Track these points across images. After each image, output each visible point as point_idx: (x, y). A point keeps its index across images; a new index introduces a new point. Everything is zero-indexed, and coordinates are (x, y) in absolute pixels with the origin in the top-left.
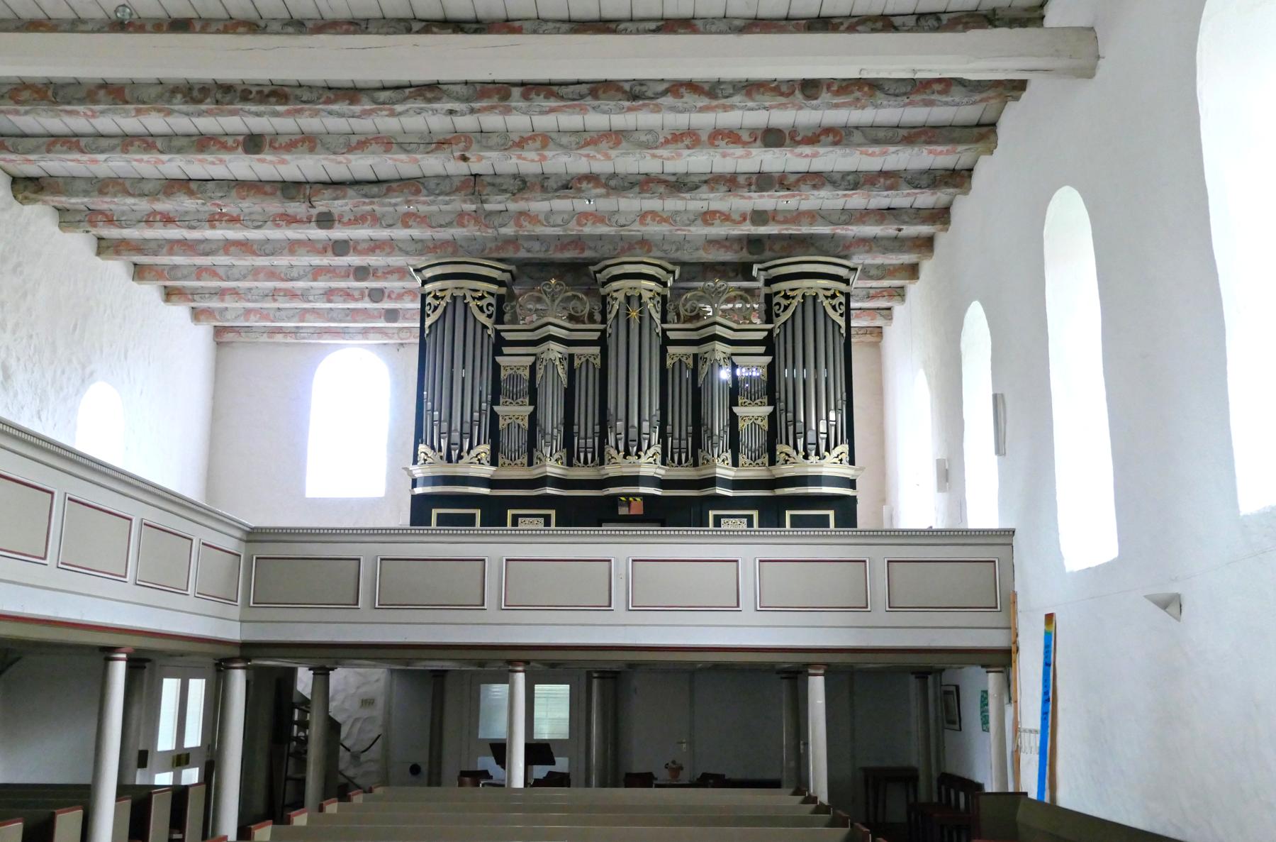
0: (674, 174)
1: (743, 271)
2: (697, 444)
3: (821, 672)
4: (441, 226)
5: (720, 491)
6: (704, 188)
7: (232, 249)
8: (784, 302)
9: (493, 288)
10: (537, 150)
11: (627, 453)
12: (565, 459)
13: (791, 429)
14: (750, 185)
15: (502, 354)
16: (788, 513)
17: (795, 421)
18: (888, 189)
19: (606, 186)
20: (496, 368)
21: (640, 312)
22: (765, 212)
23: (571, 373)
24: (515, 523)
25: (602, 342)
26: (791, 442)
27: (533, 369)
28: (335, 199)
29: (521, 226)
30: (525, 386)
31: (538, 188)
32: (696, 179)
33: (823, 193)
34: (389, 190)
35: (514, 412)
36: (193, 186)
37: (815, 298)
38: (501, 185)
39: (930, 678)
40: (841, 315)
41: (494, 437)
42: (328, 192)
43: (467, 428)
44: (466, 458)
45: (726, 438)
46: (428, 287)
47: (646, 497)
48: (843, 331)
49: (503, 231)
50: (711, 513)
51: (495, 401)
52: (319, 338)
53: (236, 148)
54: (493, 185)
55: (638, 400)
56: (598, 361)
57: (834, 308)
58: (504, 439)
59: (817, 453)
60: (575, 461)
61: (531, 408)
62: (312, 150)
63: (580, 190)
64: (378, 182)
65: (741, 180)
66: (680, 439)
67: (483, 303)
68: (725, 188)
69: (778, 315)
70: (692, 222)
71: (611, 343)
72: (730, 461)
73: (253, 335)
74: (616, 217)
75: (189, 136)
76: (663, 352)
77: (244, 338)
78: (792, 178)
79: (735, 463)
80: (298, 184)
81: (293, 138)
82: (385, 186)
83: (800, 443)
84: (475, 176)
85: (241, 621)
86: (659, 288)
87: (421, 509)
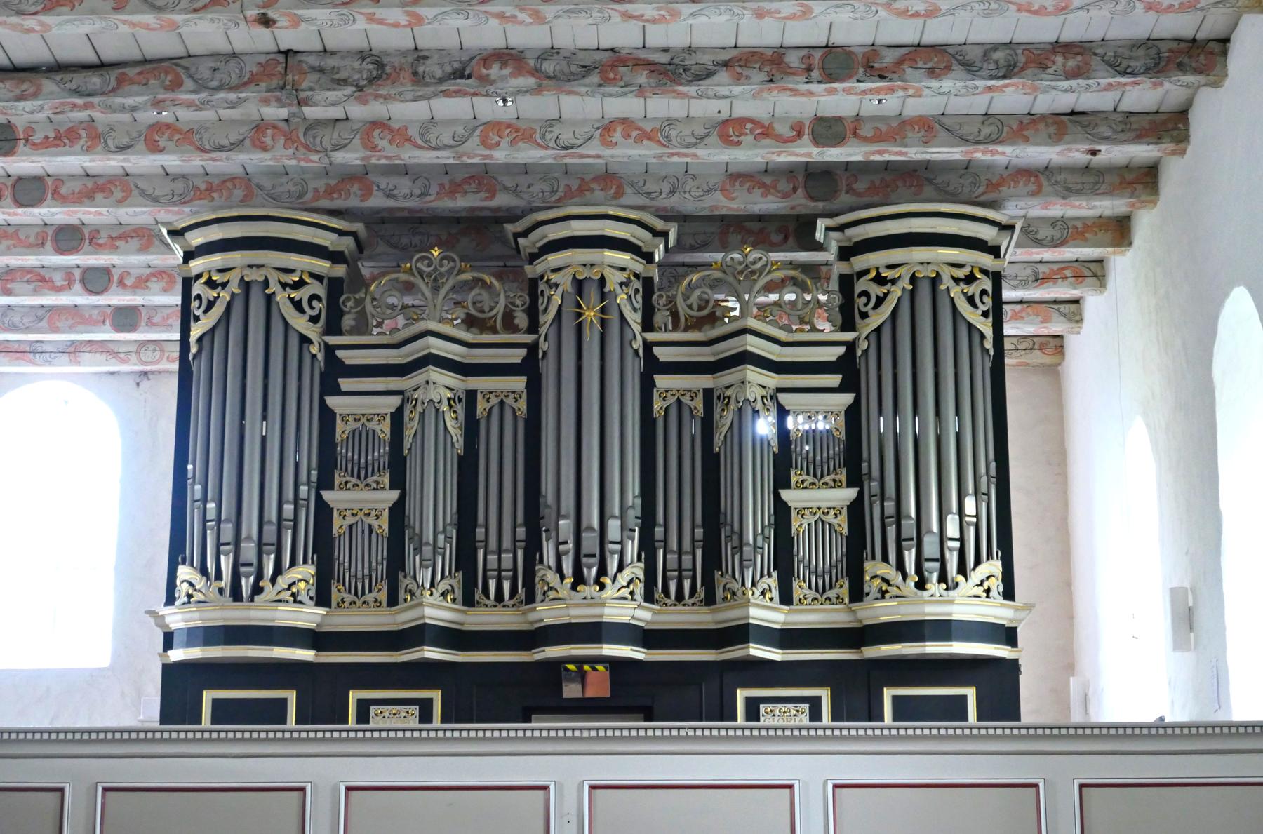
1: (799, 231)
2: (713, 561)
4: (220, 149)
5: (757, 651)
6: (723, 76)
8: (876, 290)
9: (322, 266)
11: (579, 579)
12: (459, 594)
13: (891, 531)
14: (809, 69)
15: (338, 392)
16: (208, 696)
17: (899, 515)
19: (536, 72)
20: (327, 417)
22: (839, 120)
23: (471, 427)
24: (363, 717)
25: (530, 367)
26: (892, 557)
27: (397, 419)
28: (20, 98)
30: (381, 453)
31: (406, 76)
32: (706, 59)
33: (947, 84)
34: (121, 81)
37: (935, 281)
40: (985, 314)
43: (270, 533)
44: (269, 592)
45: (768, 549)
46: (197, 265)
47: (616, 665)
48: (989, 344)
49: (340, 157)
50: (741, 694)
51: (325, 482)
54: (321, 71)
55: (601, 480)
56: (522, 405)
57: (971, 300)
58: (341, 554)
59: (943, 578)
60: (478, 595)
63: (485, 80)
64: (101, 66)
65: (793, 59)
66: (680, 552)
67: (302, 294)
69: (864, 316)
70: (701, 140)
71: (547, 369)
72: (775, 593)
74: (556, 131)
78: (889, 57)
79: (786, 598)
82: (115, 73)
83: (910, 558)
84: (287, 53)
86: (638, 265)
87: (181, 690)
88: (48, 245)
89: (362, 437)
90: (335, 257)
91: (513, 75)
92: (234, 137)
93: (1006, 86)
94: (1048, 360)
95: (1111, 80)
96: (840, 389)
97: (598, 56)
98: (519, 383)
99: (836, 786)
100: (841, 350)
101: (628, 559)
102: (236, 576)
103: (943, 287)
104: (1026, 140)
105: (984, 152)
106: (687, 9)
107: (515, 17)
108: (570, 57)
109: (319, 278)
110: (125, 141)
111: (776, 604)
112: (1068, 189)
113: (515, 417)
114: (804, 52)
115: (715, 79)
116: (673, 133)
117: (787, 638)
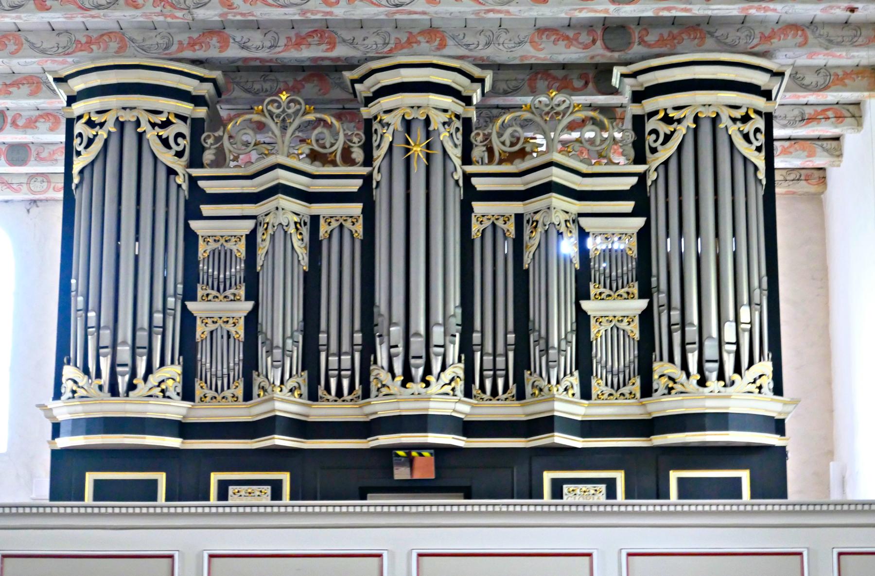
2: (523, 362)
5: (561, 439)
8: (664, 129)
9: (186, 108)
11: (408, 377)
13: (677, 337)
15: (200, 217)
21: (428, 146)
23: (315, 247)
27: (251, 239)
30: (238, 269)
37: (715, 121)
40: (759, 149)
44: (142, 388)
45: (571, 351)
46: (79, 108)
47: (440, 451)
51: (190, 294)
55: (423, 290)
56: (359, 228)
67: (169, 133)
69: (654, 151)
71: (380, 197)
72: (577, 390)
76: (466, 212)
79: (586, 394)
87: (66, 473)
89: (221, 257)
90: (198, 101)
96: (633, 214)
98: (356, 209)
100: (634, 180)
103: (722, 126)
109: (183, 119)
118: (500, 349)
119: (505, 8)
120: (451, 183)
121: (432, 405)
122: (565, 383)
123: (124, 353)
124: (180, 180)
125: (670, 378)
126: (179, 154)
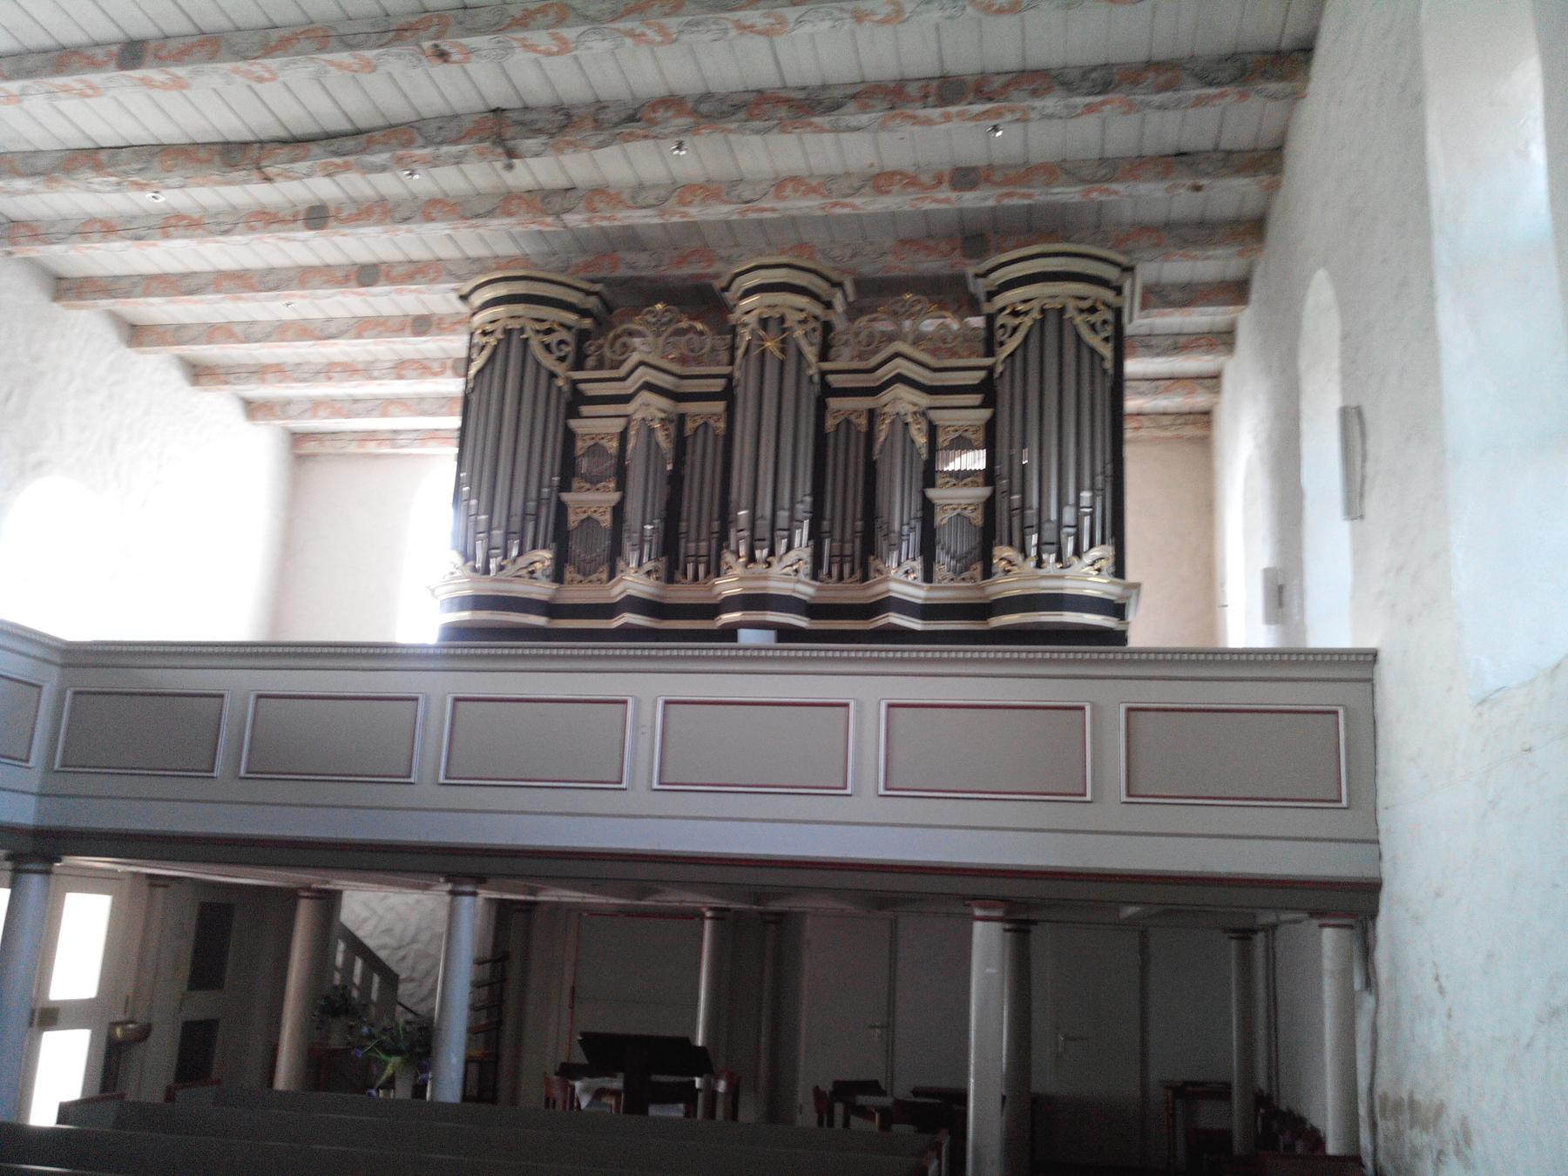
0: (804, 88)
3: (998, 913)
4: (477, 216)
6: (851, 106)
7: (225, 283)
9: (570, 318)
10: (547, 27)
11: (752, 559)
12: (662, 574)
13: (1016, 521)
14: (926, 96)
15: (578, 416)
17: (1023, 507)
18: (1161, 89)
19: (694, 112)
20: (570, 437)
21: (783, 341)
22: (973, 169)
26: (1017, 541)
27: (623, 437)
28: (293, 161)
29: (594, 210)
31: (589, 123)
32: (837, 93)
34: (370, 142)
35: (591, 502)
36: (103, 156)
37: (1062, 310)
38: (533, 122)
39: (1259, 939)
40: (1106, 339)
41: (561, 538)
42: (285, 151)
43: (516, 527)
45: (915, 537)
46: (478, 319)
48: (1109, 365)
51: (565, 486)
52: (423, 446)
53: (106, 63)
54: (521, 123)
56: (722, 425)
57: (1093, 327)
58: (576, 548)
59: (1059, 559)
60: (678, 576)
61: (616, 496)
62: (212, 57)
63: (653, 122)
64: (358, 133)
65: (912, 89)
66: (842, 541)
67: (552, 339)
68: (886, 105)
69: (1002, 344)
70: (856, 191)
71: (739, 391)
72: (919, 574)
73: (338, 444)
74: (740, 188)
75: (45, 51)
76: (821, 409)
77: (328, 447)
78: (998, 82)
79: (928, 577)
80: (245, 145)
81: (188, 40)
82: (365, 136)
84: (494, 111)
85: (41, 795)
86: (817, 309)
88: (408, 330)
89: (596, 450)
90: (584, 313)
91: (676, 116)
92: (489, 207)
93: (1103, 103)
94: (1198, 432)
95: (1197, 92)
96: (982, 406)
97: (747, 97)
98: (719, 407)
99: (890, 706)
100: (982, 374)
101: (797, 543)
102: (487, 563)
103: (1067, 316)
104: (1136, 178)
105: (1101, 191)
106: (791, 13)
107: (643, 34)
108: (722, 99)
109: (569, 328)
110: (407, 214)
111: (919, 582)
112: (1186, 241)
113: (716, 436)
114: (921, 83)
115: (844, 110)
116: (834, 187)
117: (927, 611)
118: (848, 536)
119: (849, 200)
120: (805, 381)
121: (771, 584)
122: (907, 565)
123: (498, 534)
124: (560, 382)
125: (1010, 562)
126: (562, 359)
